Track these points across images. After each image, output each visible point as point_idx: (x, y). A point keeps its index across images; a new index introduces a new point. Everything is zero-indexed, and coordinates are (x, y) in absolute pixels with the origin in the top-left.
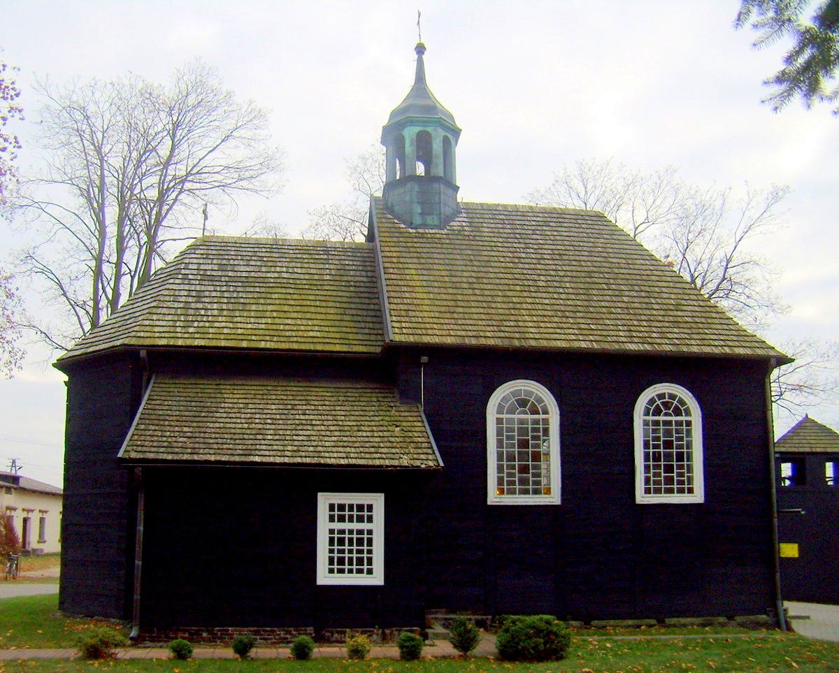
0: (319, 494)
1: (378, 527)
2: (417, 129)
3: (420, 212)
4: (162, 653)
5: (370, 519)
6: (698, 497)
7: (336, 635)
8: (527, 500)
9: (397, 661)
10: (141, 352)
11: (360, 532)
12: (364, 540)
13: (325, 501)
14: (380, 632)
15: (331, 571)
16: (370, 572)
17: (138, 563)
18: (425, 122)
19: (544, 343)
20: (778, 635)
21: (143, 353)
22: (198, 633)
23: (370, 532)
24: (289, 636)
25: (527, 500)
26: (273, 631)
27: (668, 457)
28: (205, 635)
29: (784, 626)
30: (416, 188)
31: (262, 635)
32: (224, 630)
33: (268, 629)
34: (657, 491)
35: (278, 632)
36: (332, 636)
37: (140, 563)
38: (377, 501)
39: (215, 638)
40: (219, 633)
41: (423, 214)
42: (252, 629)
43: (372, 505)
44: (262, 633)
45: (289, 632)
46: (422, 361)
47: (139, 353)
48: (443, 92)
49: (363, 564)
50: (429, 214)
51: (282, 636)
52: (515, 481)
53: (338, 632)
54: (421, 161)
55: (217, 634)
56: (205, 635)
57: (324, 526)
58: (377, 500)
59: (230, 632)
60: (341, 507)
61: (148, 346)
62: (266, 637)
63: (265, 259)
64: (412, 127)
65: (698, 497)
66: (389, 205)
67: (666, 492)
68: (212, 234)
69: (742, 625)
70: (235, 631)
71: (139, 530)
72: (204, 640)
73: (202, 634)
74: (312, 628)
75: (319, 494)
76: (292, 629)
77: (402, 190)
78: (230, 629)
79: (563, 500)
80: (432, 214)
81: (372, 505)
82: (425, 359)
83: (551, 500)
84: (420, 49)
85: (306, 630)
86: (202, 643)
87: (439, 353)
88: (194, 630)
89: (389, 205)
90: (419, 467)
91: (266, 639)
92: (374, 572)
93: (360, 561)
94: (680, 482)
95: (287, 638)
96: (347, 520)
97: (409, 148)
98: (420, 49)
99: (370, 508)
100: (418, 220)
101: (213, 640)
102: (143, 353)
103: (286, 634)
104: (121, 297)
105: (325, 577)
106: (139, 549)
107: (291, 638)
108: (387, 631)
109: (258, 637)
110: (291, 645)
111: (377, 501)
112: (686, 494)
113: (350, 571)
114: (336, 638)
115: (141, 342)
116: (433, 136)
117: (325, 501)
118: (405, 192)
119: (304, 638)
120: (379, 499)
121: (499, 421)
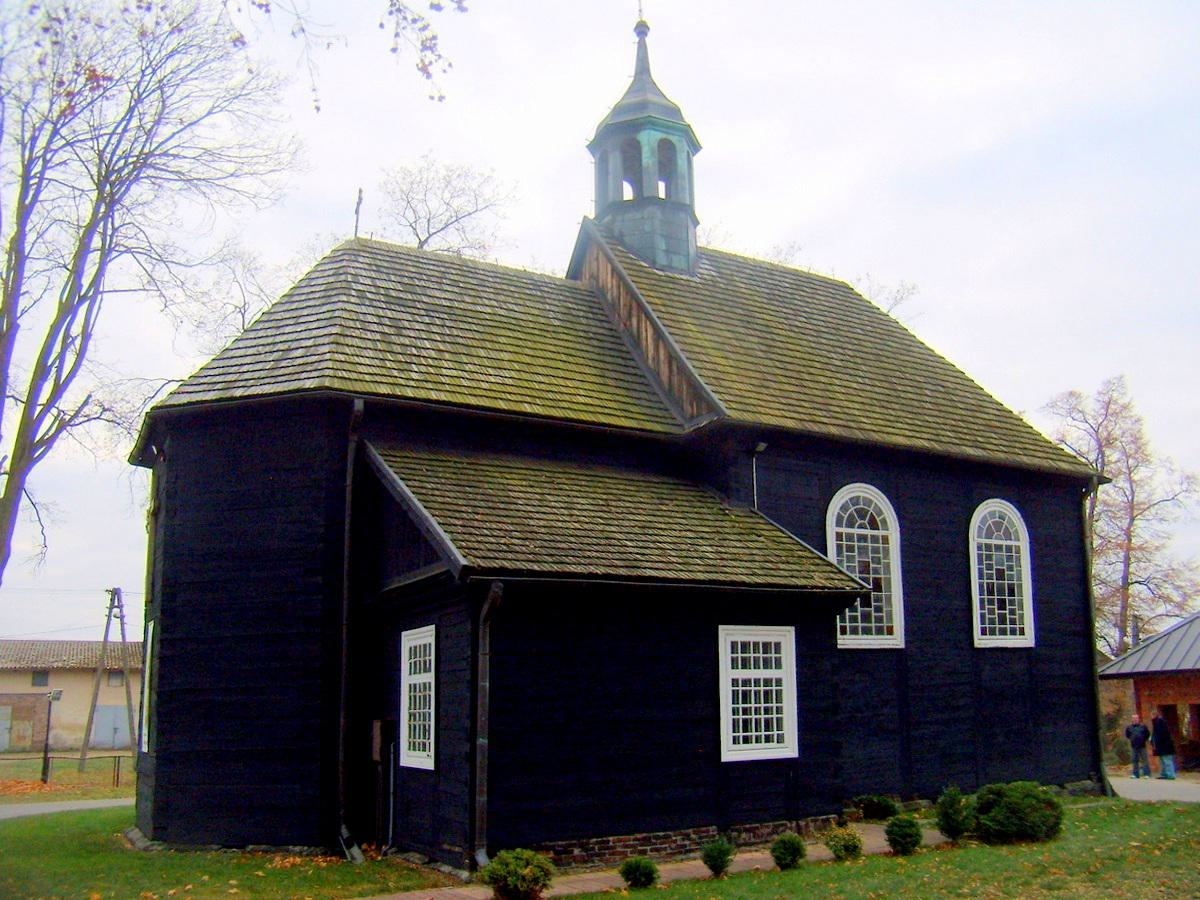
0: (721, 627)
1: (788, 674)
2: (659, 135)
3: (664, 248)
4: (605, 878)
5: (778, 665)
6: (1028, 640)
7: (744, 835)
8: (872, 642)
9: (768, 872)
10: (356, 401)
11: (767, 682)
12: (771, 693)
13: (729, 635)
14: (794, 824)
15: (735, 741)
16: (780, 739)
17: (482, 741)
18: (668, 127)
19: (876, 437)
20: (1103, 801)
21: (359, 405)
22: (567, 850)
23: (779, 682)
24: (687, 842)
25: (872, 642)
26: (667, 837)
27: (1001, 591)
28: (577, 851)
29: (1110, 793)
30: (659, 214)
31: (655, 844)
32: (604, 842)
33: (661, 834)
34: (992, 632)
35: (674, 838)
36: (739, 836)
37: (486, 741)
38: (785, 637)
39: (592, 856)
40: (596, 847)
41: (667, 252)
42: (639, 836)
43: (780, 643)
44: (653, 841)
45: (687, 837)
46: (758, 449)
47: (352, 402)
48: (670, 83)
49: (771, 729)
50: (675, 253)
51: (679, 843)
52: (882, 617)
53: (747, 831)
54: (627, 181)
55: (593, 849)
56: (577, 851)
57: (727, 675)
58: (785, 636)
59: (611, 844)
60: (745, 646)
61: (365, 393)
62: (658, 846)
63: (461, 285)
64: (653, 132)
65: (1028, 640)
66: (616, 233)
67: (733, 659)
68: (369, 238)
69: (1073, 793)
70: (620, 841)
71: (484, 687)
72: (575, 859)
73: (572, 852)
74: (714, 827)
75: (721, 627)
76: (691, 831)
77: (639, 216)
78: (611, 838)
79: (907, 642)
80: (679, 254)
81: (780, 643)
82: (762, 447)
83: (894, 642)
84: (642, 29)
85: (708, 831)
86: (574, 865)
87: (778, 438)
88: (561, 846)
89: (616, 233)
90: (844, 589)
91: (657, 850)
92: (786, 739)
93: (768, 727)
94: (1013, 622)
95: (685, 846)
96: (752, 667)
97: (648, 159)
98: (642, 29)
99: (778, 646)
100: (662, 260)
101: (588, 859)
102: (359, 405)
103: (683, 839)
104: (19, 332)
105: (788, 748)
106: (483, 718)
107: (690, 845)
108: (802, 823)
109: (648, 848)
110: (770, 845)
111: (785, 637)
112: (1009, 637)
113: (758, 740)
114: (744, 839)
115: (359, 387)
116: (678, 149)
117: (729, 635)
118: (643, 218)
119: (790, 834)
120: (788, 637)
121: (839, 536)
